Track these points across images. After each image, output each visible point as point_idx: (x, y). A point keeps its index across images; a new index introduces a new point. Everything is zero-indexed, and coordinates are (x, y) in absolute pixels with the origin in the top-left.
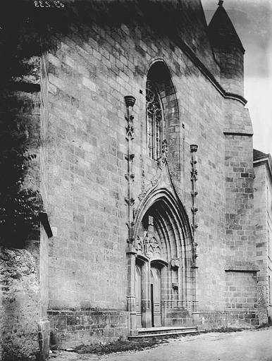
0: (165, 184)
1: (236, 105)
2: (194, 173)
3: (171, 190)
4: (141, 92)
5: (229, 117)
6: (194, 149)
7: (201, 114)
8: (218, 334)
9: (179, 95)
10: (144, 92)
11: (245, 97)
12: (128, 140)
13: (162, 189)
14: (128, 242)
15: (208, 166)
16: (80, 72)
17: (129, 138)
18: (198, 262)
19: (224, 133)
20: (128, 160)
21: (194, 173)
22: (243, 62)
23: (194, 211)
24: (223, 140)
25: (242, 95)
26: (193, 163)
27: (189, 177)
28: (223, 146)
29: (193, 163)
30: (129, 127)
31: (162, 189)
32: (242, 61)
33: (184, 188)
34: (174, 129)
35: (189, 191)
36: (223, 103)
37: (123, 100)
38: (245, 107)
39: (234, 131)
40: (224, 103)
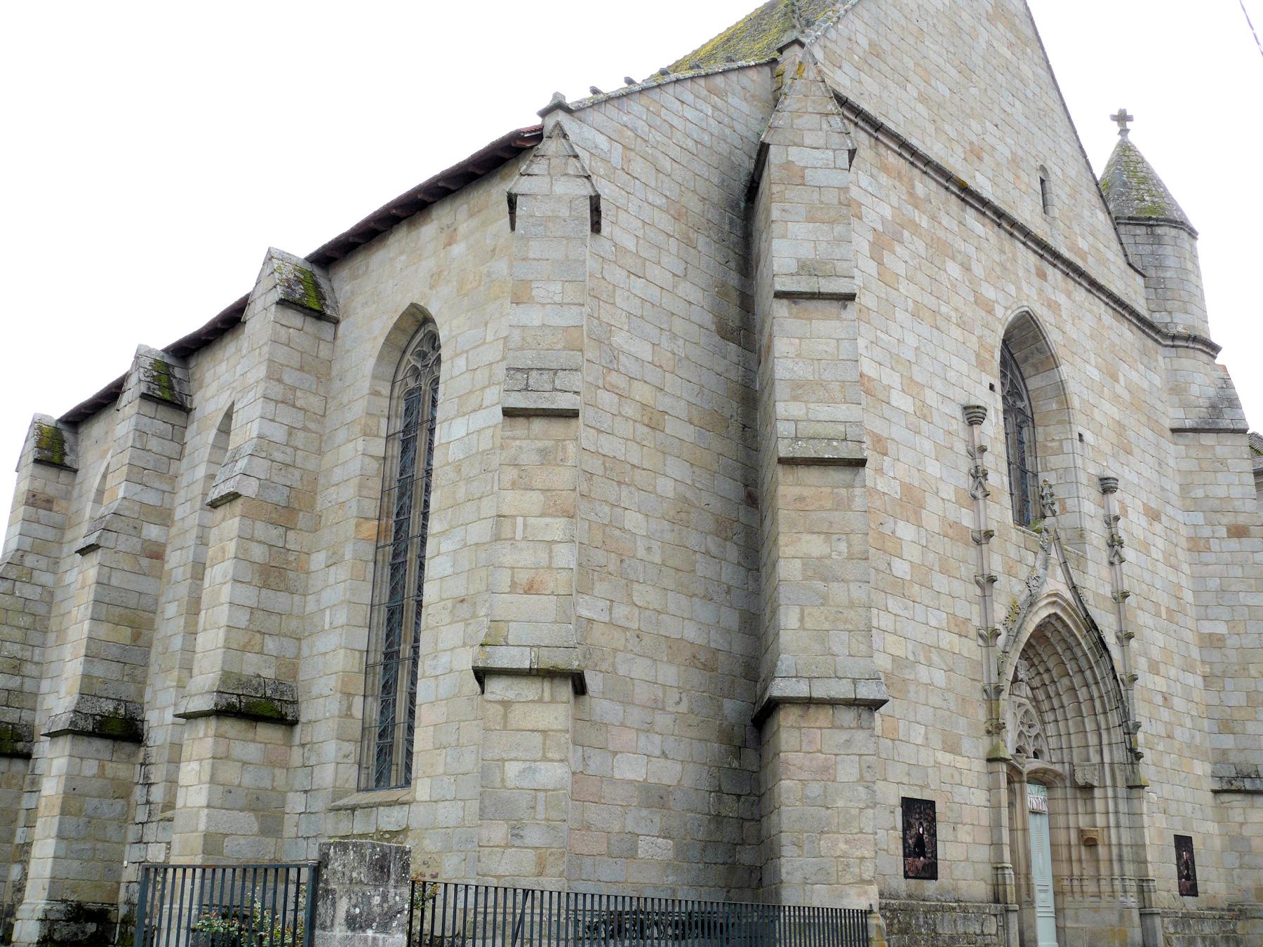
0: (1056, 583)
1: (1192, 362)
2: (1114, 543)
3: (1068, 595)
4: (992, 387)
5: (1177, 389)
6: (1107, 486)
7: (1116, 398)
8: (819, 692)
9: (1065, 370)
10: (998, 386)
11: (1215, 338)
12: (975, 497)
13: (1049, 595)
14: (989, 732)
15: (1144, 521)
16: (885, 382)
17: (979, 494)
18: (1146, 771)
19: (1174, 431)
20: (978, 543)
21: (1114, 543)
22: (1196, 256)
23: (1126, 637)
24: (1173, 450)
25: (1204, 335)
26: (1111, 521)
27: (1104, 555)
28: (1172, 462)
29: (1111, 521)
30: (977, 471)
31: (1049, 595)
32: (1194, 257)
33: (1097, 582)
34: (1061, 446)
35: (1107, 591)
36: (1160, 358)
37: (958, 413)
38: (1217, 361)
39: (934, 149)
40: (1162, 357)
